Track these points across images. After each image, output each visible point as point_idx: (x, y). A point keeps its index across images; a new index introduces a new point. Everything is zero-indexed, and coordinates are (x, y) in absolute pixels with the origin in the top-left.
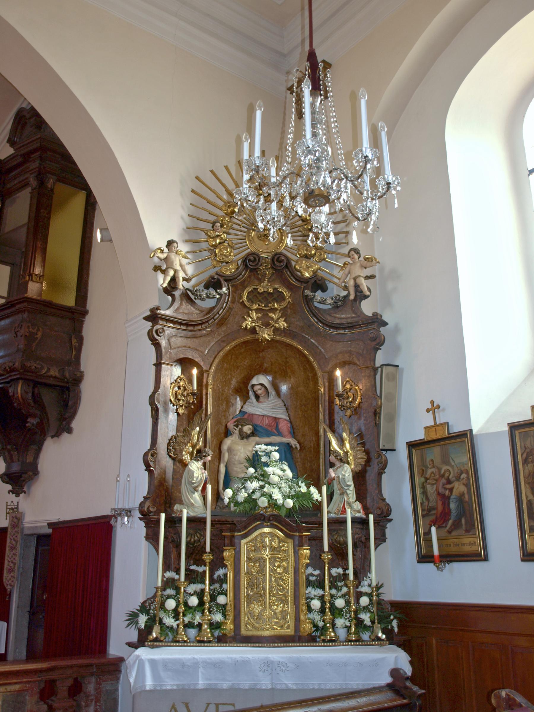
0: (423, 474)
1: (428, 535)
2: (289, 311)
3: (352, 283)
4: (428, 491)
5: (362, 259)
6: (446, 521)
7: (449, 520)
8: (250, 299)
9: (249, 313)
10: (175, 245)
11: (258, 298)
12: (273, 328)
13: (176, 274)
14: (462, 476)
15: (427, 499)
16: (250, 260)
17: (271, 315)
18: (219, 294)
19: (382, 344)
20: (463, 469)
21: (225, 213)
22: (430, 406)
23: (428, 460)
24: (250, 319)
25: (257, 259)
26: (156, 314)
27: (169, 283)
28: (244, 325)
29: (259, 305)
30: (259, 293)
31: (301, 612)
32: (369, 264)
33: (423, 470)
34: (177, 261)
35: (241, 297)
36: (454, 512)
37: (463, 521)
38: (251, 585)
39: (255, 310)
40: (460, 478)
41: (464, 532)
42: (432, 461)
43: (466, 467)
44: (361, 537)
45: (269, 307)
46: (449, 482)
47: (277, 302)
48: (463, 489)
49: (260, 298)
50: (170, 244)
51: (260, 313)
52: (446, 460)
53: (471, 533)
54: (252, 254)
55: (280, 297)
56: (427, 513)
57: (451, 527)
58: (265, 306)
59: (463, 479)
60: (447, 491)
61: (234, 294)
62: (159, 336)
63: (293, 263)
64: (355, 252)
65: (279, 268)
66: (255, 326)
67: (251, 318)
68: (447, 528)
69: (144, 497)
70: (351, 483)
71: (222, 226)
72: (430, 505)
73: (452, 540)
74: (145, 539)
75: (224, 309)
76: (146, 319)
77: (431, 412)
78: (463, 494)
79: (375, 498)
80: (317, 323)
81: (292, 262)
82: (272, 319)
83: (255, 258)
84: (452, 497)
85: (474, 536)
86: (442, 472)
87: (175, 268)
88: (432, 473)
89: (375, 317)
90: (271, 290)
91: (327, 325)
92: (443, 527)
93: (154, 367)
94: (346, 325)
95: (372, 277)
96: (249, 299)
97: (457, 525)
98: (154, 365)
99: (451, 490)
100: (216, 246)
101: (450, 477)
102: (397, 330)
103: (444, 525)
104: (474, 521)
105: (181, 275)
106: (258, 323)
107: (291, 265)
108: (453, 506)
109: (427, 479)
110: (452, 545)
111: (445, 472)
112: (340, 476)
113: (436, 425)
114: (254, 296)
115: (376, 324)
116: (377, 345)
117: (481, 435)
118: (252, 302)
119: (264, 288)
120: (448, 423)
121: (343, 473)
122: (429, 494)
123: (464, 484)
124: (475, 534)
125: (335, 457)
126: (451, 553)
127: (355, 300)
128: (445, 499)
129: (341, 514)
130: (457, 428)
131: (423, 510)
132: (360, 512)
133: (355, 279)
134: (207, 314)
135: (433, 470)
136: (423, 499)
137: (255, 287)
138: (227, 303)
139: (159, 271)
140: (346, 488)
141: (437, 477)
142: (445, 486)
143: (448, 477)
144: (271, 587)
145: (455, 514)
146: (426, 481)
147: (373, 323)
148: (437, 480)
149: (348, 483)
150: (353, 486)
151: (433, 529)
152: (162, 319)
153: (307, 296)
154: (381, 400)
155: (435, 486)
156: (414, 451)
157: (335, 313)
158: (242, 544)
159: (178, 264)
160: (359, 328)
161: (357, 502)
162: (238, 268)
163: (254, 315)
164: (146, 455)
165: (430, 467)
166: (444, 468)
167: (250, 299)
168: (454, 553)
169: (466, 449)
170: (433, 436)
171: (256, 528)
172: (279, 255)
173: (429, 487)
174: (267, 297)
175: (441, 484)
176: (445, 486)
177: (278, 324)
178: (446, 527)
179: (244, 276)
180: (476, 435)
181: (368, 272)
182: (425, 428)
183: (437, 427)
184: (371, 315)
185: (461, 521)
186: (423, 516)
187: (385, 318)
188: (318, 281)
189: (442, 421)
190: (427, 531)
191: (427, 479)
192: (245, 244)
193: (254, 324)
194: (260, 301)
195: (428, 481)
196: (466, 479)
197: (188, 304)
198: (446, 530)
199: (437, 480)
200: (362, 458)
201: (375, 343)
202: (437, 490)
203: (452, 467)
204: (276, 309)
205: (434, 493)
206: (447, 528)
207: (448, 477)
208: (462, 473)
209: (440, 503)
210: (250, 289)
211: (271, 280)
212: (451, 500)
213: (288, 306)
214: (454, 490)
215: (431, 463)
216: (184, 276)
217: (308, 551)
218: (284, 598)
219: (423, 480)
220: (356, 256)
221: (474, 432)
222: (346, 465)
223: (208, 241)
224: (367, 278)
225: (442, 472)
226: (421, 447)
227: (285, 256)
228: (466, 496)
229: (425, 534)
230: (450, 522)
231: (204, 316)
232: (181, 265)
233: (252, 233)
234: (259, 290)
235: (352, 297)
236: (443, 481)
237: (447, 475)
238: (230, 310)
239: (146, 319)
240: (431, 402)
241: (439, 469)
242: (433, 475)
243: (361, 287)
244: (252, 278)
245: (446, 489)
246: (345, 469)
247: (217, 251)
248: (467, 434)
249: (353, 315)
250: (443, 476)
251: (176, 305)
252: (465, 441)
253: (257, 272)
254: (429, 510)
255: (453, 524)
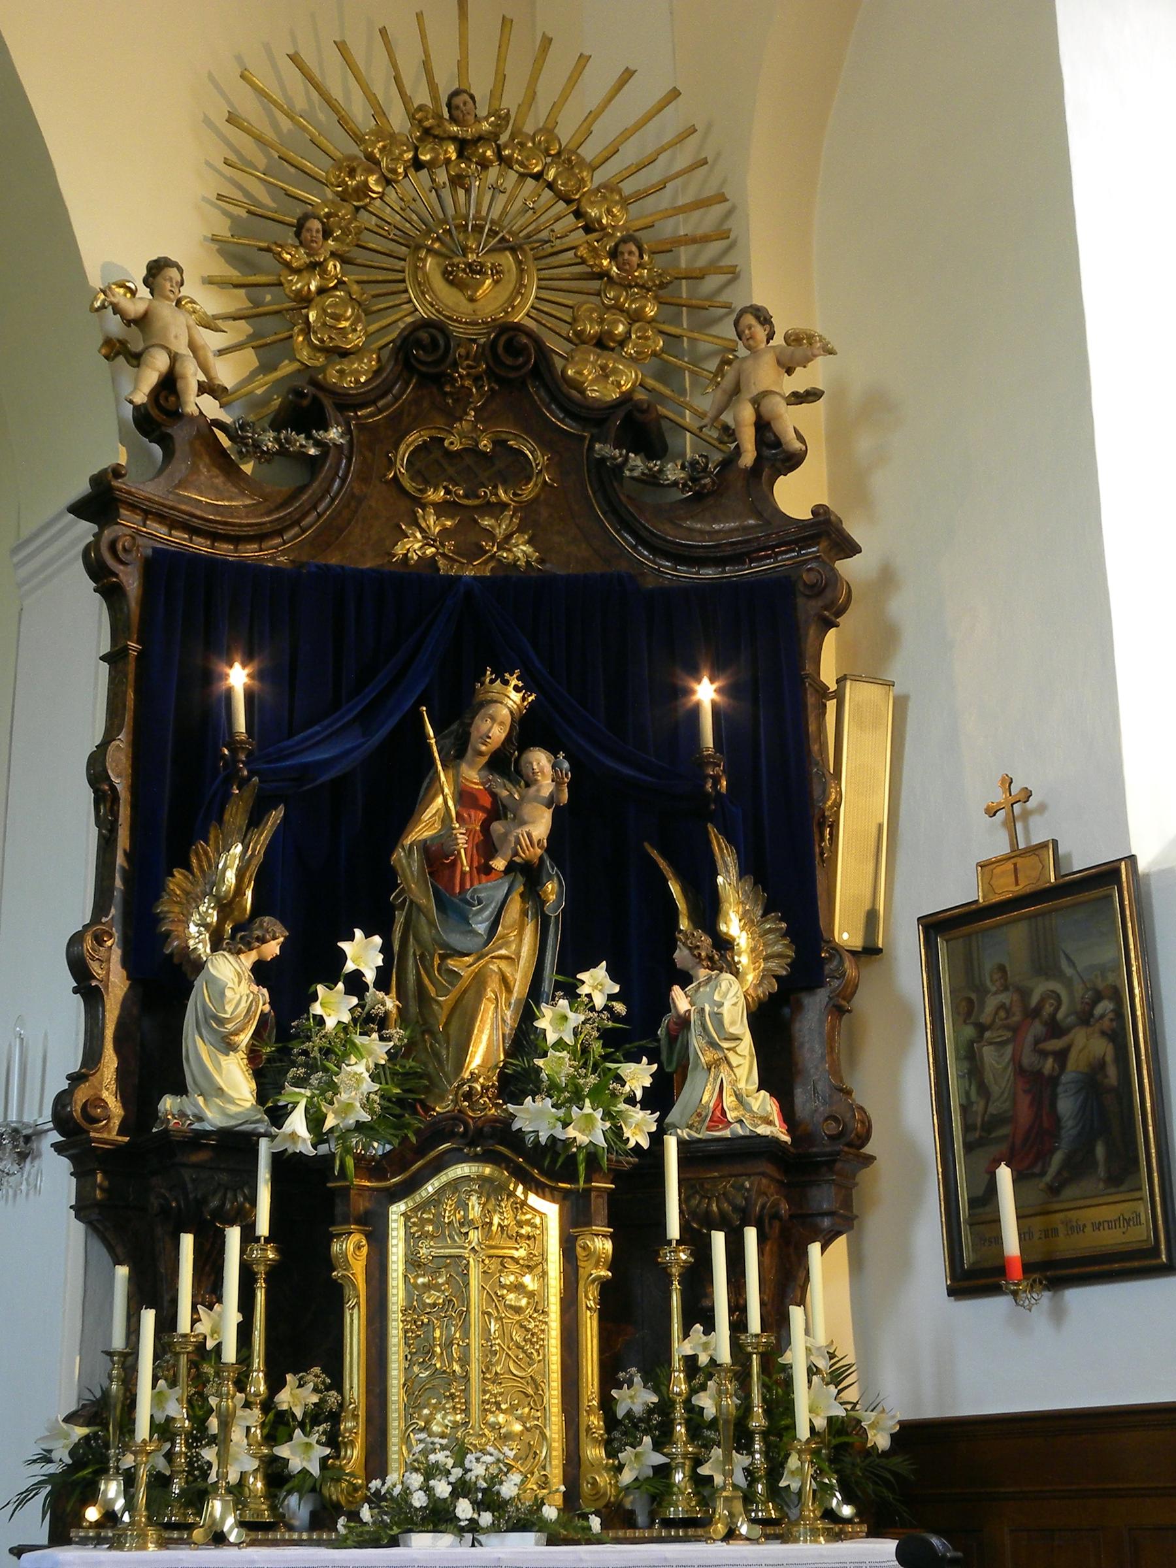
0: (969, 1014)
1: (984, 1205)
2: (545, 512)
3: (747, 414)
4: (987, 1066)
5: (778, 340)
6: (1044, 1156)
7: (1052, 1151)
8: (419, 472)
9: (415, 513)
10: (173, 273)
11: (444, 470)
12: (492, 564)
13: (178, 365)
14: (1099, 1010)
15: (984, 1090)
16: (419, 344)
17: (486, 522)
18: (318, 443)
19: (841, 612)
20: (1101, 985)
21: (337, 194)
22: (999, 796)
23: (989, 965)
24: (419, 535)
25: (442, 342)
26: (111, 489)
27: (155, 393)
28: (399, 550)
29: (448, 492)
30: (448, 454)
31: (583, 1434)
32: (799, 352)
33: (970, 1001)
34: (177, 328)
35: (391, 464)
36: (1070, 1123)
37: (1100, 1151)
38: (420, 1351)
39: (435, 505)
40: (1091, 1015)
41: (1101, 1186)
42: (1002, 969)
43: (1111, 978)
44: (776, 1204)
45: (478, 497)
46: (1055, 1029)
47: (505, 483)
48: (1101, 1047)
49: (451, 471)
50: (156, 269)
51: (452, 518)
52: (1045, 963)
53: (1122, 1188)
54: (425, 324)
55: (518, 470)
56: (981, 1137)
57: (1059, 1173)
58: (466, 496)
59: (1102, 1017)
60: (1050, 1061)
61: (368, 454)
62: (122, 562)
63: (559, 363)
64: (758, 318)
65: (512, 375)
66: (434, 555)
67: (422, 530)
68: (1048, 1179)
69: (69, 1077)
70: (741, 1028)
71: (327, 234)
72: (992, 1110)
73: (1061, 1216)
74: (72, 1212)
75: (333, 499)
76: (80, 509)
77: (1001, 815)
78: (1102, 1065)
79: (819, 1088)
80: (634, 548)
81: (556, 359)
82: (490, 534)
83: (434, 340)
84: (1064, 1078)
85: (1137, 1195)
86: (1034, 1001)
87: (174, 348)
88: (1002, 1006)
89: (821, 518)
90: (485, 444)
91: (667, 556)
92: (1034, 1175)
93: (105, 667)
94: (729, 551)
95: (811, 396)
96: (416, 472)
97: (1078, 1166)
98: (103, 658)
99: (1062, 1056)
100: (305, 300)
101: (1060, 1015)
102: (887, 579)
103: (1037, 1170)
104: (1136, 1150)
105: (192, 376)
106: (443, 545)
107: (550, 366)
108: (1066, 1106)
109: (981, 1028)
110: (1062, 1230)
111: (1042, 1001)
112: (707, 1008)
113: (1016, 853)
114: (433, 462)
115: (824, 544)
116: (826, 608)
117: (1162, 872)
118: (427, 482)
119: (462, 435)
120: (1055, 842)
121: (716, 998)
122: (989, 1077)
123: (1103, 1033)
124: (1140, 1189)
125: (690, 949)
126: (1058, 1256)
127: (756, 470)
128: (1041, 1087)
129: (709, 1129)
130: (1083, 856)
131: (967, 1128)
132: (770, 1123)
133: (756, 402)
134: (278, 508)
135: (1004, 998)
136: (967, 1094)
137: (434, 433)
138: (343, 480)
139: (121, 360)
140: (725, 1045)
141: (1016, 1018)
142: (1041, 1046)
143: (1053, 1016)
144: (489, 1352)
145: (1074, 1132)
146: (981, 1036)
147: (812, 540)
148: (1015, 1029)
149: (732, 1030)
150: (748, 1039)
151: (1004, 1174)
152: (133, 507)
153: (603, 460)
154: (839, 784)
155: (1009, 1050)
156: (941, 944)
157: (692, 518)
158: (392, 1217)
159: (184, 340)
160: (768, 557)
161: (763, 1092)
162: (377, 373)
163: (432, 523)
164: (76, 940)
165: (994, 989)
166: (1040, 988)
167: (419, 472)
168: (1068, 1255)
169: (1114, 922)
170: (1006, 889)
171: (438, 1166)
172: (512, 333)
173: (988, 1054)
174: (472, 467)
175: (1030, 1039)
176: (1041, 1046)
177: (510, 550)
178: (1043, 1174)
179: (396, 399)
180: (1147, 875)
181: (799, 381)
182: (982, 866)
183: (1018, 860)
184: (807, 515)
185: (1091, 1151)
186: (969, 1147)
187: (855, 530)
188: (638, 415)
189: (1036, 840)
190: (980, 1192)
191: (981, 1028)
192: (405, 296)
193: (430, 551)
194: (451, 480)
195: (987, 1034)
196: (1111, 1016)
197: (215, 471)
198: (1042, 1185)
199: (1015, 1029)
200: (780, 956)
201: (820, 603)
202: (1016, 1060)
203: (1068, 983)
204: (504, 506)
205: (1005, 1068)
206: (1048, 1179)
207: (1053, 1016)
208: (1098, 997)
209: (1024, 1101)
210: (414, 439)
211: (485, 415)
212: (1060, 1089)
213: (542, 497)
214: (1073, 1055)
215: (996, 977)
216: (203, 378)
217: (608, 1246)
218: (530, 1391)
219: (969, 1031)
220: (760, 333)
221: (1142, 865)
222: (727, 976)
223: (281, 284)
224: (798, 398)
225: (1034, 1001)
226: (966, 929)
227: (529, 334)
228: (1112, 1071)
229: (973, 1202)
230: (1057, 1159)
231: (269, 513)
232: (192, 346)
233: (424, 260)
234: (446, 443)
235: (748, 458)
236: (1037, 1028)
237: (1048, 1009)
238: (353, 504)
239: (80, 509)
240: (1003, 781)
241: (1024, 994)
242: (1002, 1014)
243: (776, 426)
244: (425, 404)
245: (1044, 1054)
246: (724, 985)
247: (312, 316)
248: (1117, 871)
249: (751, 522)
250: (1036, 1013)
251: (180, 466)
252: (1111, 896)
253: (441, 387)
254: (992, 1123)
255: (1067, 1163)
